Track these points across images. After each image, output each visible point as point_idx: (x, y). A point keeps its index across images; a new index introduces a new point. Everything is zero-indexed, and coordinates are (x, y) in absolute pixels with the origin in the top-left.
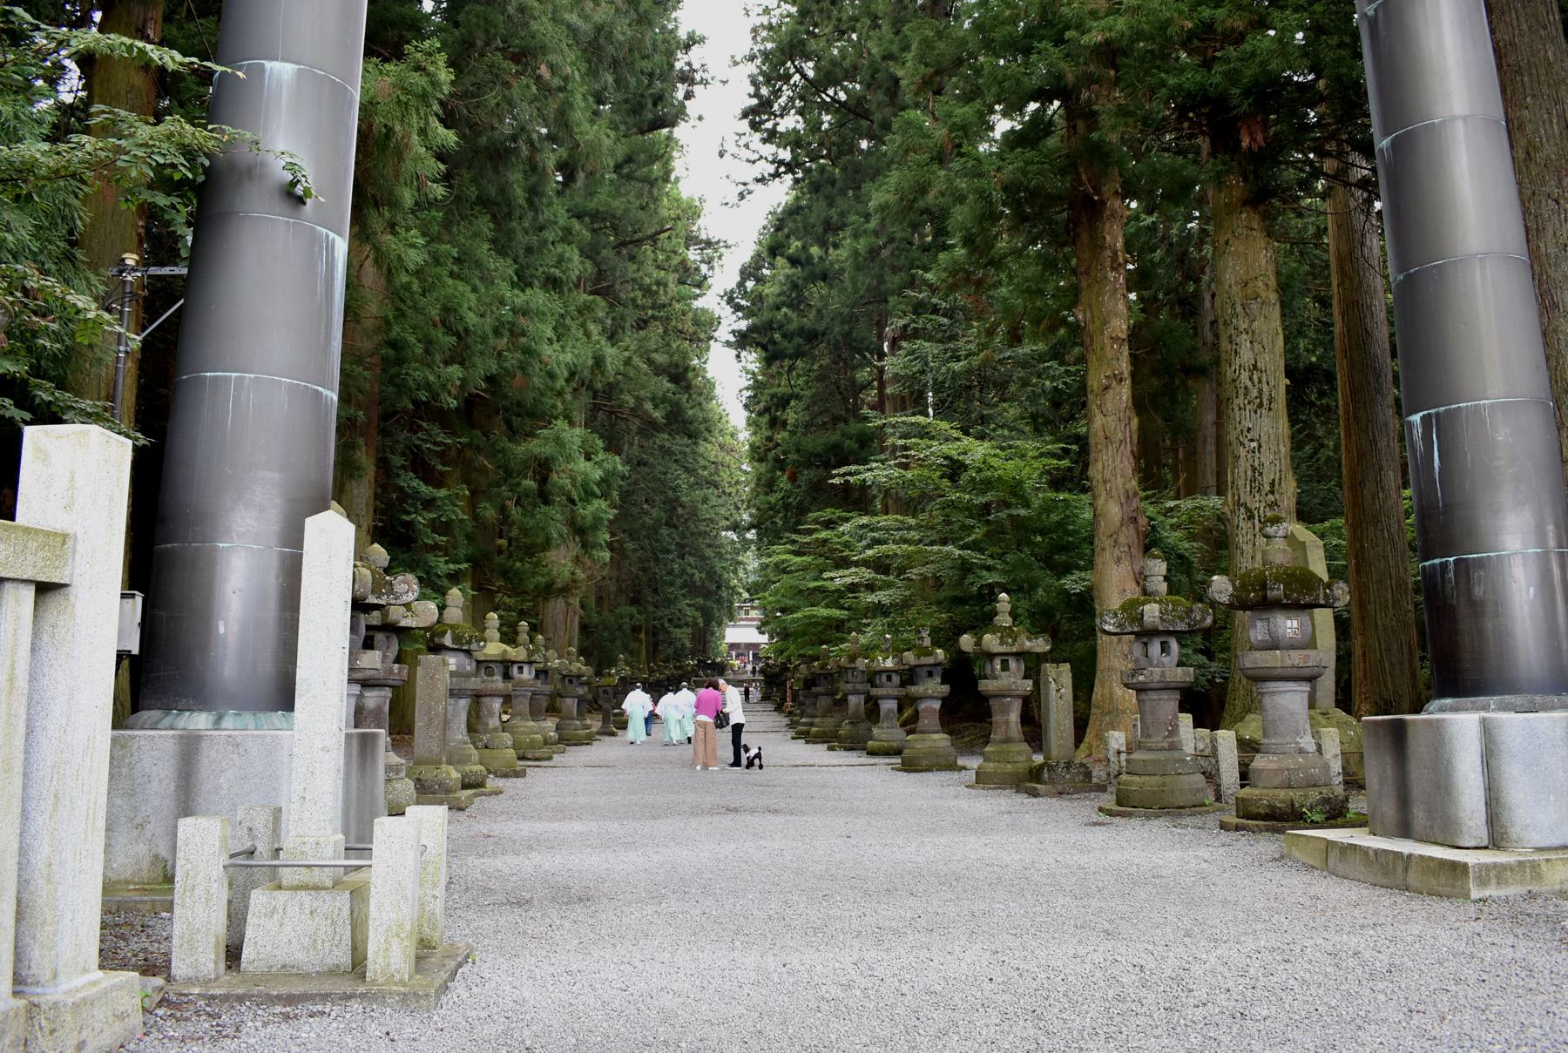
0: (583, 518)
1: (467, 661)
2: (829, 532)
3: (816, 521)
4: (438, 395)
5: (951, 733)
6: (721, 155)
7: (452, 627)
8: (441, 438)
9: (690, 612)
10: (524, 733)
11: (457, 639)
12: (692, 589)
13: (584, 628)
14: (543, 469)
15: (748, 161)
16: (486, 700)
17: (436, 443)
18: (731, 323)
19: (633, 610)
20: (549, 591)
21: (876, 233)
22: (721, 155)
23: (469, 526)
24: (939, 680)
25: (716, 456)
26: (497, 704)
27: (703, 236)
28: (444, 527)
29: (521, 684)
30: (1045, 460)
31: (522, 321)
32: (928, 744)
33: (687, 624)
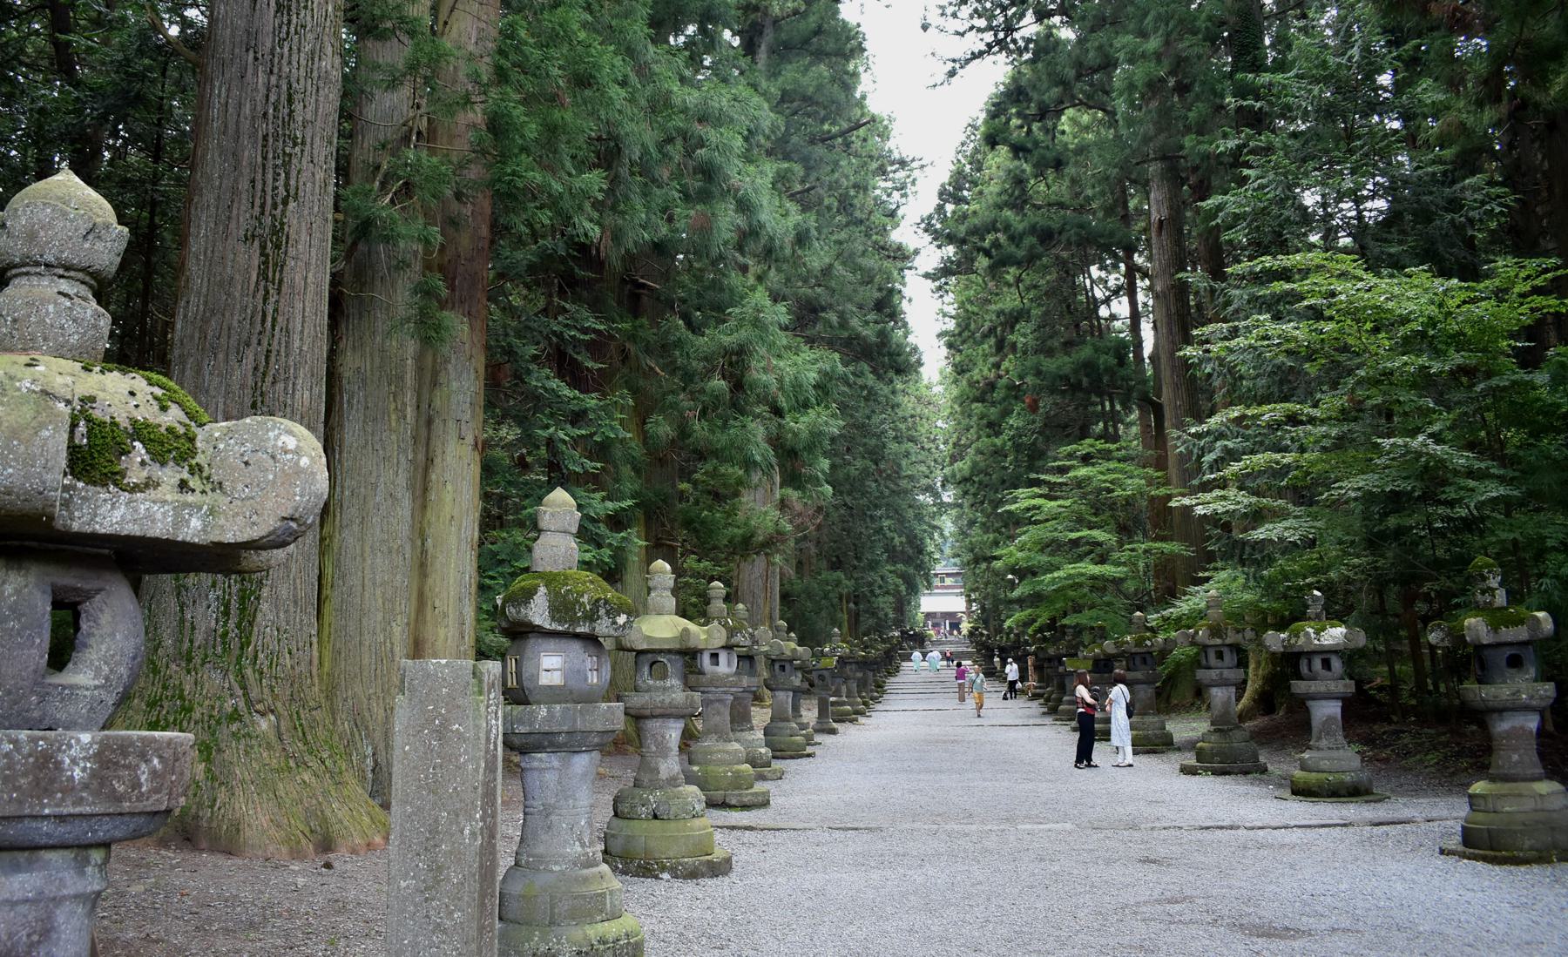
0: (796, 435)
1: (590, 662)
2: (1090, 468)
3: (1070, 456)
4: (570, 218)
5: (1368, 741)
6: (925, 27)
7: (550, 579)
8: (591, 323)
9: (892, 579)
10: (722, 762)
11: (562, 607)
12: (893, 555)
13: (785, 597)
14: (735, 363)
15: (957, 33)
16: (653, 725)
17: (585, 331)
18: (931, 256)
19: (840, 574)
20: (746, 546)
21: (1158, 57)
22: (925, 27)
23: (638, 451)
24: (1532, 672)
25: (914, 409)
26: (673, 732)
27: (896, 155)
28: (601, 451)
29: (717, 681)
30: (1538, 301)
31: (699, 129)
32: (1529, 805)
33: (887, 593)
